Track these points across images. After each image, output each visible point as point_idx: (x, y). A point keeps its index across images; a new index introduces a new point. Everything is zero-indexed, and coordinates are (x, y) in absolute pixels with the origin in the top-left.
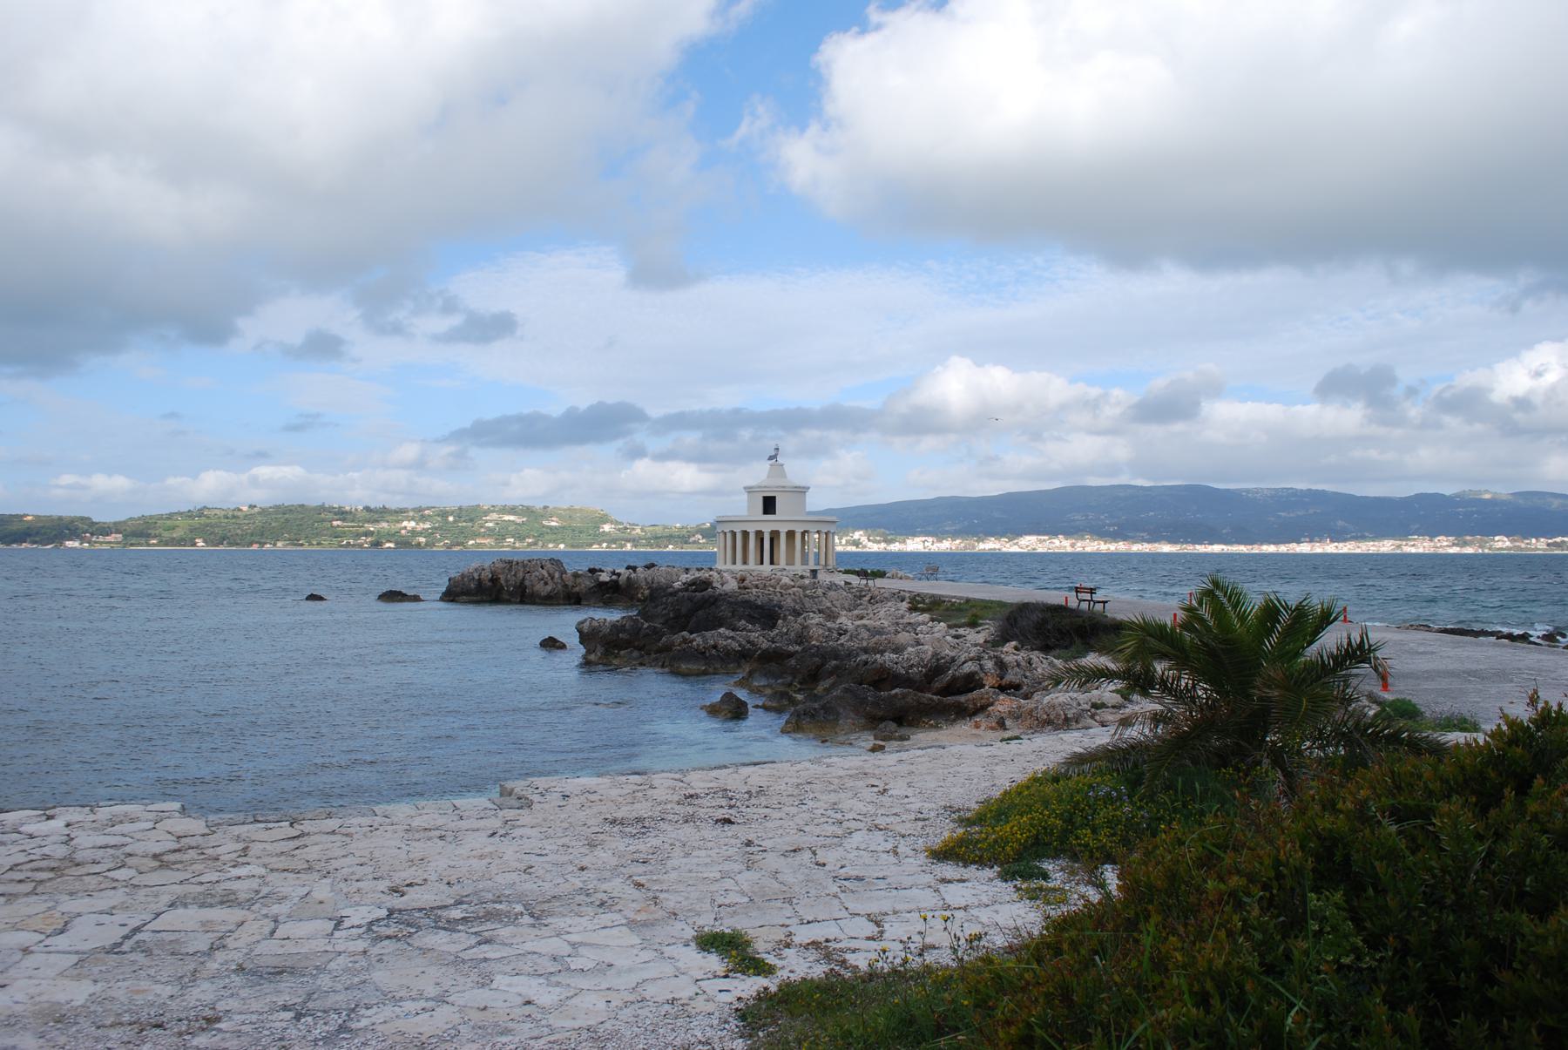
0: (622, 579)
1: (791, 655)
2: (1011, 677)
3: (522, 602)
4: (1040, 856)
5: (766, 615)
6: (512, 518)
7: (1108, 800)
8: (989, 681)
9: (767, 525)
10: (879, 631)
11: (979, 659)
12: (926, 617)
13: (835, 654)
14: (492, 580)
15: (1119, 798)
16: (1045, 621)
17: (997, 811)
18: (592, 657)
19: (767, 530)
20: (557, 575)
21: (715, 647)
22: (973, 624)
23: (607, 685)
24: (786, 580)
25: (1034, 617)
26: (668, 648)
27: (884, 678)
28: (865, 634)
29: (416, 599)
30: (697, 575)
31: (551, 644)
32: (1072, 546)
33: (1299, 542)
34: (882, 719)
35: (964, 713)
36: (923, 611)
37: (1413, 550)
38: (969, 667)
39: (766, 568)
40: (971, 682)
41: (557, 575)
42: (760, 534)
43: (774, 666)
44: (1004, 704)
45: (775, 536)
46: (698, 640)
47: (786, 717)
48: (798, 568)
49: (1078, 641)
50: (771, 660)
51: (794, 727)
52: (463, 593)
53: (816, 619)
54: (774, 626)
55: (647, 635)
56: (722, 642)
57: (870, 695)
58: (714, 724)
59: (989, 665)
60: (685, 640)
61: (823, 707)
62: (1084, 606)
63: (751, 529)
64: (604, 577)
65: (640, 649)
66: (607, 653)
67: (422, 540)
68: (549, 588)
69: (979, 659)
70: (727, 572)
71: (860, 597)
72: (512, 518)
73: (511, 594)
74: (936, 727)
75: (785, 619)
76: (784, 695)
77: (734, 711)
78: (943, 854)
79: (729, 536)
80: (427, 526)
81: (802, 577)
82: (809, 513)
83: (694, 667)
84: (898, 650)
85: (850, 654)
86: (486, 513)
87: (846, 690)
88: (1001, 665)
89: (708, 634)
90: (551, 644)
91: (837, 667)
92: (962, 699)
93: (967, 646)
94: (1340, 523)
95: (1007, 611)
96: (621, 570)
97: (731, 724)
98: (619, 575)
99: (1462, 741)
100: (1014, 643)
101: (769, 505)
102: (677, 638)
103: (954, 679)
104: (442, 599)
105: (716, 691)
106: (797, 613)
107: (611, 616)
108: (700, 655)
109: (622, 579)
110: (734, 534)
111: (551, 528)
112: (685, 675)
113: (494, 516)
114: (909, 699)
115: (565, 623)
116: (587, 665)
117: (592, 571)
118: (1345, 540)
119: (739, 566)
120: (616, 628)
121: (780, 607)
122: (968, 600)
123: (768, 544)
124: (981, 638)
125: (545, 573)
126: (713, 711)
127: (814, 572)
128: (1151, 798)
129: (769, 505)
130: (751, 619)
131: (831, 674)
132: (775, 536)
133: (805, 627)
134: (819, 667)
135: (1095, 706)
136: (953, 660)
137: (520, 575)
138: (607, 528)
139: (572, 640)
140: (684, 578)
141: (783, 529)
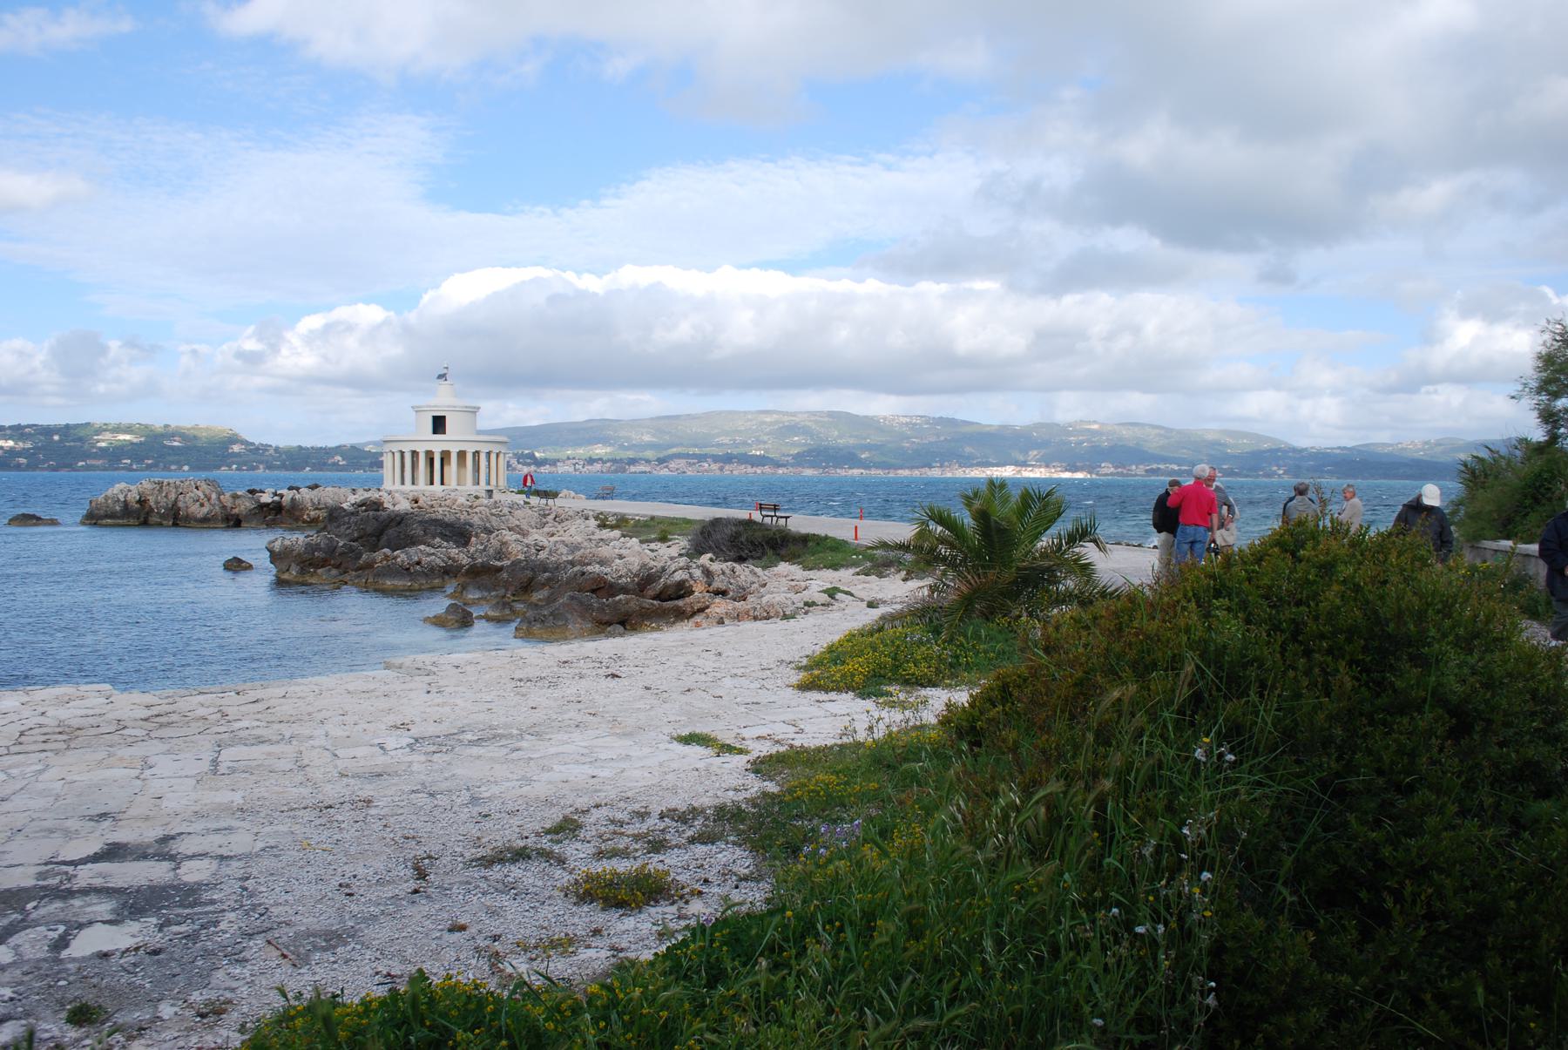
0: (286, 500)
1: (500, 569)
2: (718, 584)
3: (175, 525)
4: (891, 681)
5: (459, 533)
6: (128, 437)
7: (920, 643)
8: (699, 589)
9: (438, 445)
10: (574, 548)
11: (688, 568)
12: (617, 533)
13: (544, 567)
14: (139, 502)
15: (928, 641)
16: (738, 534)
17: (835, 655)
18: (286, 576)
19: (437, 450)
20: (214, 496)
21: (418, 563)
22: (663, 539)
23: (298, 604)
24: (462, 500)
25: (728, 531)
26: (369, 566)
27: (602, 587)
28: (564, 550)
29: (53, 522)
30: (367, 495)
31: (236, 566)
32: (721, 469)
33: (931, 467)
34: (609, 624)
35: (681, 615)
36: (612, 527)
37: (1032, 475)
38: (680, 576)
39: (437, 486)
40: (682, 590)
41: (214, 496)
42: (430, 457)
43: (485, 579)
44: (720, 606)
45: (445, 456)
46: (401, 557)
47: (514, 625)
48: (469, 487)
49: (770, 552)
50: (480, 574)
51: (526, 634)
52: (107, 516)
53: (509, 536)
54: (466, 543)
55: (341, 554)
56: (425, 560)
57: (595, 601)
58: (441, 633)
59: (697, 573)
60: (386, 557)
61: (551, 614)
62: (768, 520)
63: (421, 449)
64: (266, 498)
65: (337, 567)
66: (303, 571)
67: (22, 460)
68: (205, 510)
69: (688, 568)
70: (397, 492)
71: (545, 516)
72: (128, 437)
73: (162, 516)
74: (658, 629)
75: (477, 536)
76: (505, 605)
77: (462, 620)
78: (804, 687)
79: (398, 456)
80: (29, 445)
81: (477, 497)
82: (480, 432)
83: (399, 583)
84: (602, 563)
85: (557, 567)
86: (99, 431)
87: (572, 598)
88: (708, 573)
89: (412, 550)
90: (236, 566)
91: (549, 579)
92: (680, 603)
93: (669, 556)
94: (968, 449)
95: (698, 527)
96: (285, 492)
97: (461, 633)
98: (282, 496)
99: (621, 869)
100: (710, 555)
101: (439, 424)
102: (379, 555)
103: (666, 587)
104: (83, 523)
105: (439, 605)
106: (489, 532)
107: (298, 539)
108: (406, 571)
109: (286, 500)
110: (402, 453)
111: (173, 448)
112: (385, 592)
113: (108, 436)
114: (632, 604)
115: (254, 544)
116: (280, 583)
117: (252, 492)
118: (971, 466)
119: (408, 486)
120: (311, 548)
121: (471, 525)
122: (653, 518)
123: (436, 464)
124: (674, 551)
125: (200, 493)
126: (438, 622)
127: (490, 492)
128: (951, 641)
129: (439, 424)
130: (444, 537)
131: (544, 585)
132: (445, 456)
133: (504, 544)
134: (531, 580)
135: (806, 604)
136: (664, 569)
137: (173, 496)
138: (236, 448)
139: (261, 559)
140: (353, 499)
141: (454, 449)
